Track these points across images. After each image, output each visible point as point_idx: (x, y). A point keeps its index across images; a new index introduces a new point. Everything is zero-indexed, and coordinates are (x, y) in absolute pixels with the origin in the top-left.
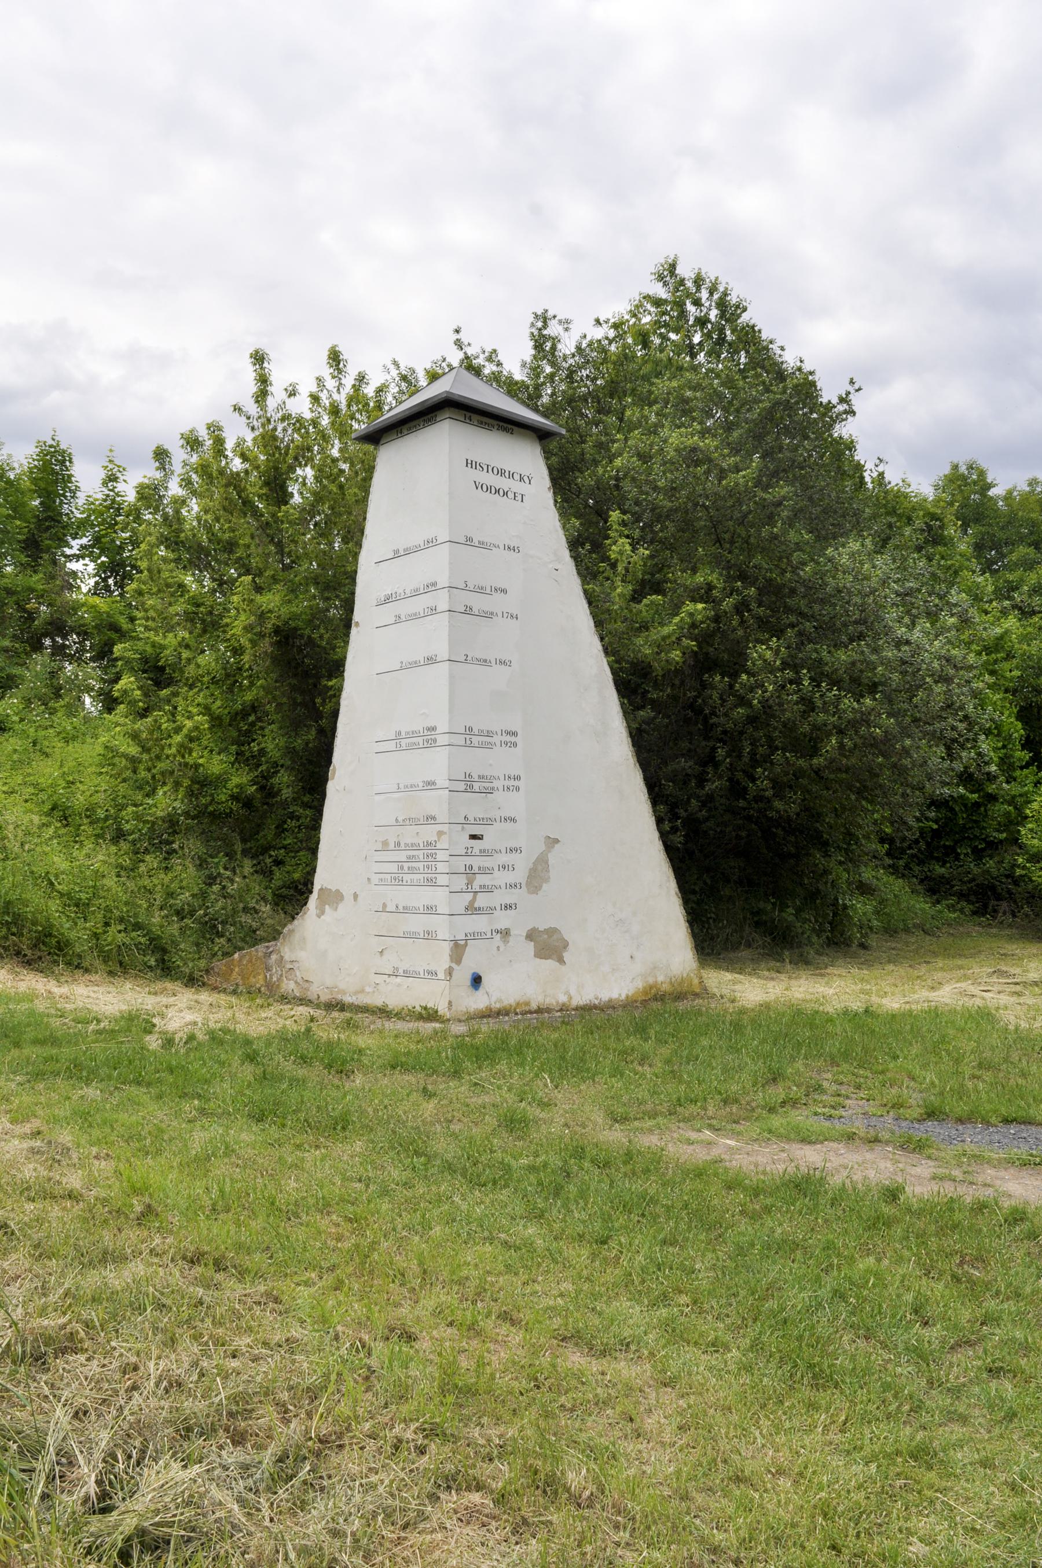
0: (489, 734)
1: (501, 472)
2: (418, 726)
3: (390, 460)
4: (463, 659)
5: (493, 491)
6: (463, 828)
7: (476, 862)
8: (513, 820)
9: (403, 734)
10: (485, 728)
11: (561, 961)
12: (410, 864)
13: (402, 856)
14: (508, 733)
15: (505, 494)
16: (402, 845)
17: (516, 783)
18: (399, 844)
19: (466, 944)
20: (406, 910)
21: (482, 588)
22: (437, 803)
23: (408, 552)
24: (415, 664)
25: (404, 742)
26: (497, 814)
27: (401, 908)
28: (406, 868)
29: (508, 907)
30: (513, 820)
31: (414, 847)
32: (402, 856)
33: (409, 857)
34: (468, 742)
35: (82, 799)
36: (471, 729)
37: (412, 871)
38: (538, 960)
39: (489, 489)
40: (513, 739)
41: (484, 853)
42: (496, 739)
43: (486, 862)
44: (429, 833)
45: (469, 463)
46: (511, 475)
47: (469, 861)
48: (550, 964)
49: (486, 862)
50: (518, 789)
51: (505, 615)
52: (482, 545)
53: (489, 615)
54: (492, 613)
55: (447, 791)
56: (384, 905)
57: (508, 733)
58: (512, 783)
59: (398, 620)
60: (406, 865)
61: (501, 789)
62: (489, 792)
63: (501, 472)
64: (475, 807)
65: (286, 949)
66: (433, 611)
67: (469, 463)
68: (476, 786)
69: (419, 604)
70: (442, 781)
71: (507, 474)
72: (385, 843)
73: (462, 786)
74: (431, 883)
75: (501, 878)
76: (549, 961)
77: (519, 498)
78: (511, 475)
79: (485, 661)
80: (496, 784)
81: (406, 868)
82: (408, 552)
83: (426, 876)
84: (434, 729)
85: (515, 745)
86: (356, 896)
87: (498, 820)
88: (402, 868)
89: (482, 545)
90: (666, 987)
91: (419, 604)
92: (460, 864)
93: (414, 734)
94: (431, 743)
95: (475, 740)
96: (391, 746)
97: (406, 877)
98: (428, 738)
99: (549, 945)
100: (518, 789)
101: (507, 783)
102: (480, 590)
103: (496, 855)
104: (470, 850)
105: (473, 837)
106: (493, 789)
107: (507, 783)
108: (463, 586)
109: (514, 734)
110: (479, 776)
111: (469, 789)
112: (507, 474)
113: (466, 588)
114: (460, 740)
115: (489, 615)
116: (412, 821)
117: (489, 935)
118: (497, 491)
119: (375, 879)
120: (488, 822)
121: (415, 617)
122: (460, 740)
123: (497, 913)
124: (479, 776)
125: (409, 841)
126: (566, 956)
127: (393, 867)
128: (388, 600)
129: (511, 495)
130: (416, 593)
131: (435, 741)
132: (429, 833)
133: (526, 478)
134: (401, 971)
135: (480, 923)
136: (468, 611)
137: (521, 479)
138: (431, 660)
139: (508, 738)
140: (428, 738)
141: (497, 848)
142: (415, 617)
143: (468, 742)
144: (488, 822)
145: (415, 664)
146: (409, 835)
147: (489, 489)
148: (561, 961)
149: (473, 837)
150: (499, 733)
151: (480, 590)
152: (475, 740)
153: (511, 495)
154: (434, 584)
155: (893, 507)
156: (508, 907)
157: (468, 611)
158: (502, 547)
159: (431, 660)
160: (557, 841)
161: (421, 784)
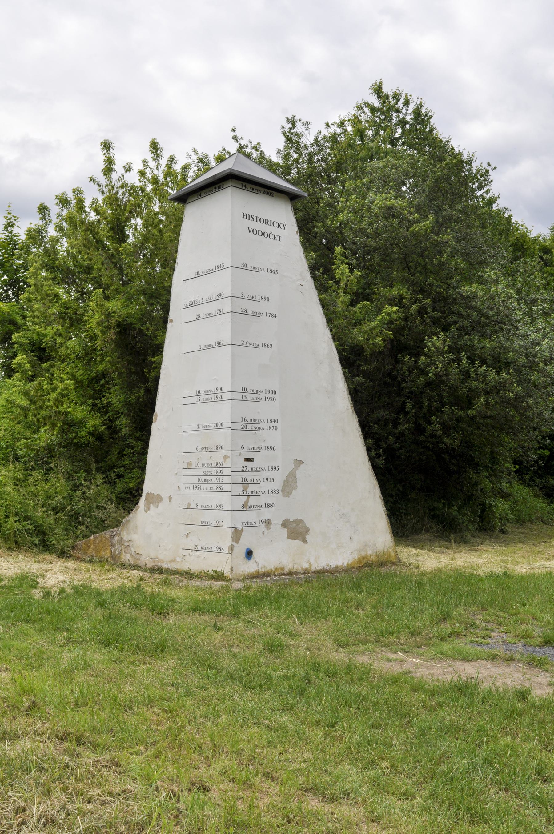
1: (266, 222)
2: (211, 387)
4: (240, 343)
5: (260, 234)
6: (240, 454)
7: (249, 476)
8: (273, 449)
9: (201, 392)
10: (255, 389)
11: (304, 541)
12: (206, 478)
13: (200, 472)
14: (270, 392)
15: (268, 236)
16: (201, 465)
17: (275, 424)
18: (198, 464)
19: (242, 530)
20: (203, 507)
22: (223, 437)
23: (205, 274)
24: (209, 347)
25: (202, 398)
26: (263, 445)
28: (203, 480)
29: (270, 505)
30: (273, 449)
31: (208, 466)
32: (200, 472)
33: (205, 473)
34: (244, 398)
36: (246, 389)
37: (207, 482)
39: (258, 232)
40: (273, 396)
41: (254, 470)
42: (262, 396)
43: (256, 476)
44: (218, 457)
46: (272, 224)
47: (244, 475)
49: (256, 476)
51: (268, 315)
52: (253, 269)
53: (257, 315)
54: (260, 314)
56: (189, 504)
57: (270, 392)
58: (272, 424)
59: (198, 318)
60: (203, 478)
62: (258, 430)
63: (266, 222)
64: (248, 440)
65: (125, 533)
68: (249, 426)
71: (269, 223)
72: (190, 464)
73: (239, 426)
74: (219, 489)
75: (265, 486)
77: (277, 238)
78: (272, 224)
79: (255, 345)
81: (203, 481)
82: (205, 274)
84: (221, 389)
88: (201, 480)
89: (253, 269)
92: (238, 477)
93: (208, 392)
94: (220, 399)
96: (194, 400)
97: (203, 486)
98: (217, 395)
99: (297, 531)
102: (252, 298)
105: (247, 460)
106: (260, 428)
108: (240, 296)
109: (274, 392)
110: (251, 420)
112: (269, 223)
116: (207, 449)
118: (263, 234)
119: (183, 487)
120: (257, 450)
123: (263, 509)
124: (251, 420)
125: (205, 462)
126: (308, 538)
127: (195, 480)
130: (210, 301)
131: (222, 397)
132: (218, 457)
133: (282, 226)
135: (251, 516)
136: (244, 312)
137: (279, 226)
138: (220, 344)
139: (270, 395)
140: (217, 395)
143: (244, 398)
144: (257, 450)
145: (209, 347)
147: (258, 232)
148: (304, 541)
149: (247, 460)
150: (264, 392)
151: (252, 298)
152: (249, 396)
154: (222, 294)
156: (270, 505)
157: (244, 312)
158: (266, 270)
160: (302, 462)
161: (213, 425)
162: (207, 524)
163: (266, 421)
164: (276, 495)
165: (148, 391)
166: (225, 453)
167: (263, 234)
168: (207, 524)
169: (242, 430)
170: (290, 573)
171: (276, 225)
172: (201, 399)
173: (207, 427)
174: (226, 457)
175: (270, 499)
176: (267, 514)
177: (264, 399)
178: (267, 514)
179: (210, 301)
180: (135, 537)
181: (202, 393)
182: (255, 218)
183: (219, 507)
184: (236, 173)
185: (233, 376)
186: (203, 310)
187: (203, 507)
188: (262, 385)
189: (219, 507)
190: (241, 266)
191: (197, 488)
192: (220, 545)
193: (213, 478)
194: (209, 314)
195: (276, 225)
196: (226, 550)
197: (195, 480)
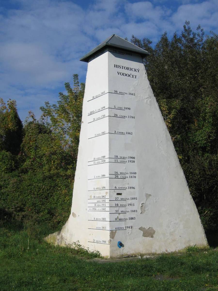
0: (124, 158)
1: (128, 69)
2: (100, 156)
3: (92, 64)
4: (114, 132)
5: (125, 75)
6: (114, 191)
7: (120, 203)
8: (134, 188)
9: (96, 159)
10: (122, 156)
13: (96, 201)
14: (131, 158)
15: (129, 76)
16: (96, 197)
17: (135, 175)
19: (116, 232)
20: (97, 220)
21: (121, 108)
22: (105, 182)
24: (99, 135)
25: (96, 162)
26: (127, 186)
27: (95, 219)
28: (97, 205)
29: (132, 219)
30: (134, 188)
31: (99, 198)
32: (96, 201)
33: (98, 201)
34: (116, 161)
36: (117, 156)
37: (99, 206)
38: (144, 237)
39: (123, 74)
40: (133, 160)
42: (127, 160)
43: (124, 203)
44: (103, 193)
46: (131, 69)
47: (117, 202)
48: (148, 239)
49: (124, 203)
50: (135, 177)
51: (130, 117)
52: (121, 93)
53: (124, 117)
54: (125, 116)
57: (131, 158)
58: (133, 175)
60: (97, 204)
61: (129, 177)
62: (124, 178)
63: (128, 69)
64: (119, 184)
65: (63, 233)
66: (104, 116)
68: (119, 176)
69: (99, 115)
70: (107, 175)
71: (130, 69)
73: (114, 176)
74: (104, 210)
75: (129, 208)
76: (148, 238)
77: (135, 77)
78: (131, 69)
79: (122, 133)
80: (127, 175)
81: (97, 205)
82: (97, 97)
83: (102, 208)
84: (104, 157)
85: (134, 162)
86: (79, 216)
87: (128, 188)
88: (96, 205)
89: (121, 93)
90: (202, 248)
91: (99, 115)
92: (114, 203)
93: (99, 159)
94: (104, 162)
95: (119, 160)
96: (92, 163)
97: (97, 208)
99: (149, 233)
100: (135, 177)
101: (131, 175)
102: (120, 109)
103: (127, 200)
104: (117, 199)
105: (118, 194)
106: (126, 177)
107: (131, 175)
108: (113, 107)
109: (134, 158)
110: (120, 173)
111: (117, 177)
112: (130, 69)
113: (115, 108)
114: (113, 160)
115: (124, 117)
116: (98, 189)
117: (125, 229)
118: (126, 75)
119: (88, 209)
120: (125, 189)
122: (113, 160)
123: (128, 221)
124: (120, 173)
125: (98, 196)
126: (154, 236)
129: (131, 76)
131: (105, 161)
132: (103, 193)
133: (137, 70)
134: (96, 241)
135: (122, 225)
136: (116, 116)
137: (135, 70)
138: (104, 133)
139: (131, 160)
141: (128, 198)
143: (116, 161)
144: (125, 189)
145: (99, 135)
147: (123, 74)
148: (152, 237)
149: (118, 194)
150: (128, 158)
151: (120, 109)
152: (119, 160)
153: (131, 76)
154: (104, 107)
156: (132, 219)
157: (116, 116)
158: (128, 94)
159: (104, 133)
160: (150, 195)
161: (101, 176)
162: (98, 229)
163: (129, 173)
164: (136, 213)
167: (126, 75)
168: (98, 229)
169: (115, 178)
170: (129, 257)
171: (133, 70)
172: (96, 163)
173: (98, 177)
175: (133, 215)
176: (130, 223)
177: (128, 161)
178: (130, 223)
182: (122, 67)
185: (110, 150)
187: (97, 220)
188: (128, 154)
189: (104, 220)
190: (113, 92)
191: (94, 210)
192: (104, 240)
194: (99, 118)
195: (133, 70)
196: (107, 243)
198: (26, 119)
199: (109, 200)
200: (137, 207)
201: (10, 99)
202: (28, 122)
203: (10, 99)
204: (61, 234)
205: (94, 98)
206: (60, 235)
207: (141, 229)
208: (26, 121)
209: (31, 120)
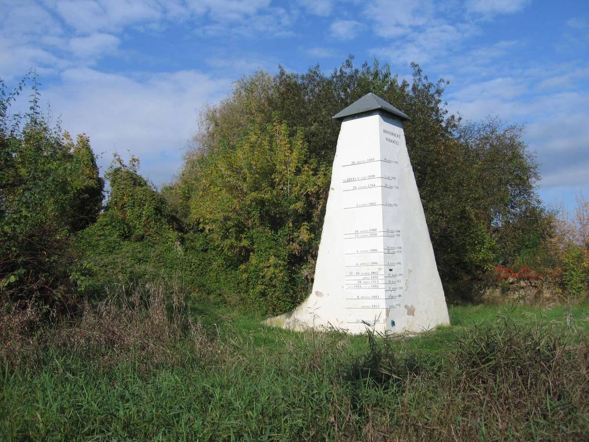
11: (413, 315)
12: (365, 281)
13: (361, 278)
18: (358, 273)
22: (379, 258)
23: (359, 163)
24: (364, 206)
28: (362, 283)
30: (400, 263)
32: (361, 278)
35: (544, 292)
37: (365, 283)
41: (394, 276)
45: (385, 131)
48: (411, 317)
55: (383, 253)
56: (358, 297)
59: (355, 188)
67: (385, 131)
72: (351, 273)
74: (376, 287)
84: (375, 230)
93: (365, 232)
96: (354, 236)
97: (362, 286)
98: (373, 233)
118: (392, 134)
121: (364, 188)
126: (415, 314)
127: (356, 282)
128: (349, 180)
130: (364, 179)
132: (375, 269)
140: (373, 233)
142: (364, 188)
145: (364, 206)
146: (363, 270)
148: (413, 315)
154: (374, 176)
155: (170, 214)
160: (411, 271)
165: (437, 254)
166: (379, 267)
168: (363, 307)
174: (380, 269)
179: (364, 179)
180: (470, 306)
181: (359, 232)
183: (375, 297)
184: (391, 120)
186: (357, 184)
189: (375, 297)
191: (358, 287)
193: (370, 281)
197: (356, 282)
198: (111, 164)
199: (384, 276)
200: (402, 284)
201: (84, 134)
202: (114, 168)
203: (84, 134)
204: (293, 315)
205: (353, 164)
206: (292, 318)
207: (406, 307)
208: (111, 168)
209: (118, 165)
